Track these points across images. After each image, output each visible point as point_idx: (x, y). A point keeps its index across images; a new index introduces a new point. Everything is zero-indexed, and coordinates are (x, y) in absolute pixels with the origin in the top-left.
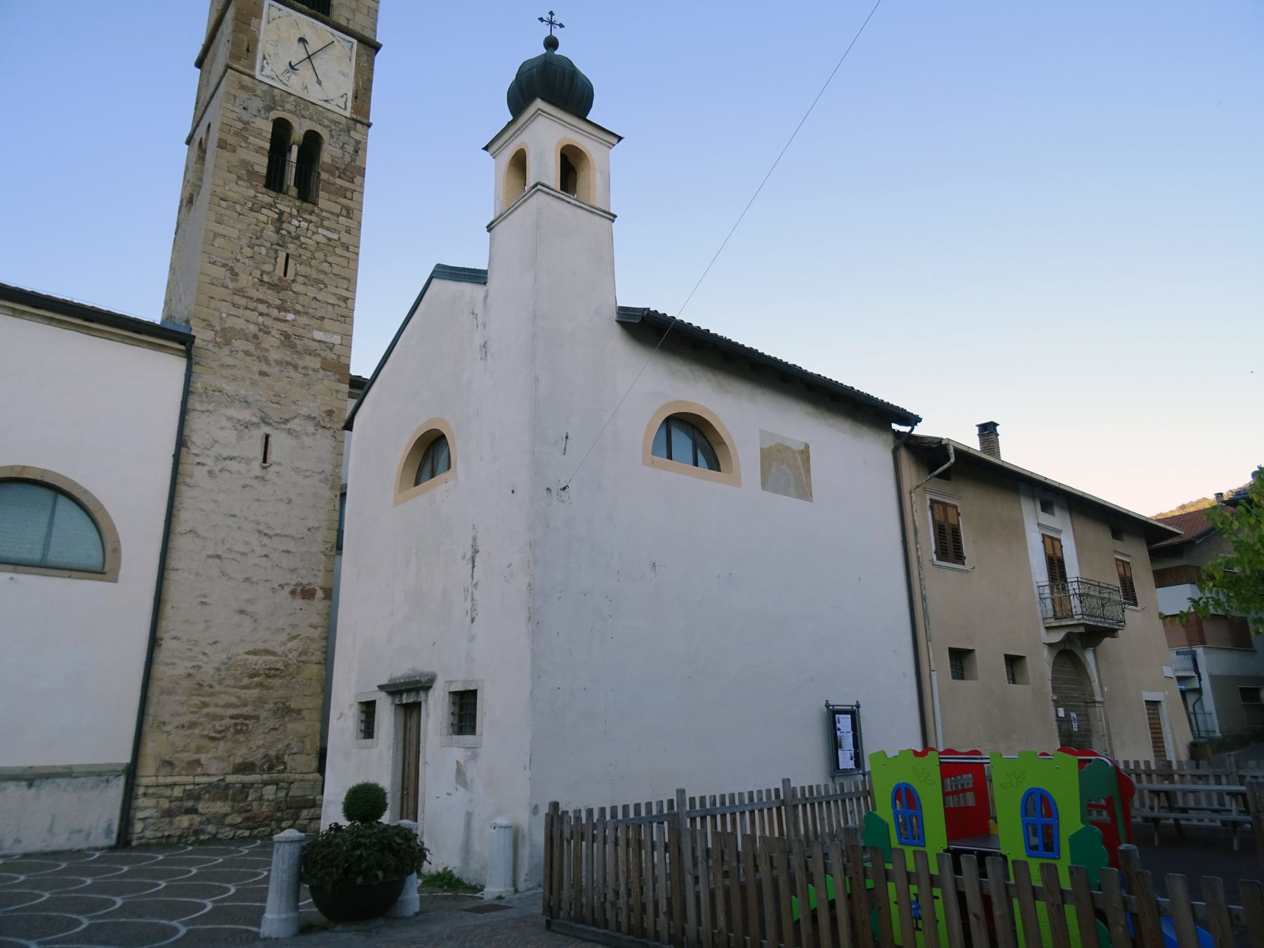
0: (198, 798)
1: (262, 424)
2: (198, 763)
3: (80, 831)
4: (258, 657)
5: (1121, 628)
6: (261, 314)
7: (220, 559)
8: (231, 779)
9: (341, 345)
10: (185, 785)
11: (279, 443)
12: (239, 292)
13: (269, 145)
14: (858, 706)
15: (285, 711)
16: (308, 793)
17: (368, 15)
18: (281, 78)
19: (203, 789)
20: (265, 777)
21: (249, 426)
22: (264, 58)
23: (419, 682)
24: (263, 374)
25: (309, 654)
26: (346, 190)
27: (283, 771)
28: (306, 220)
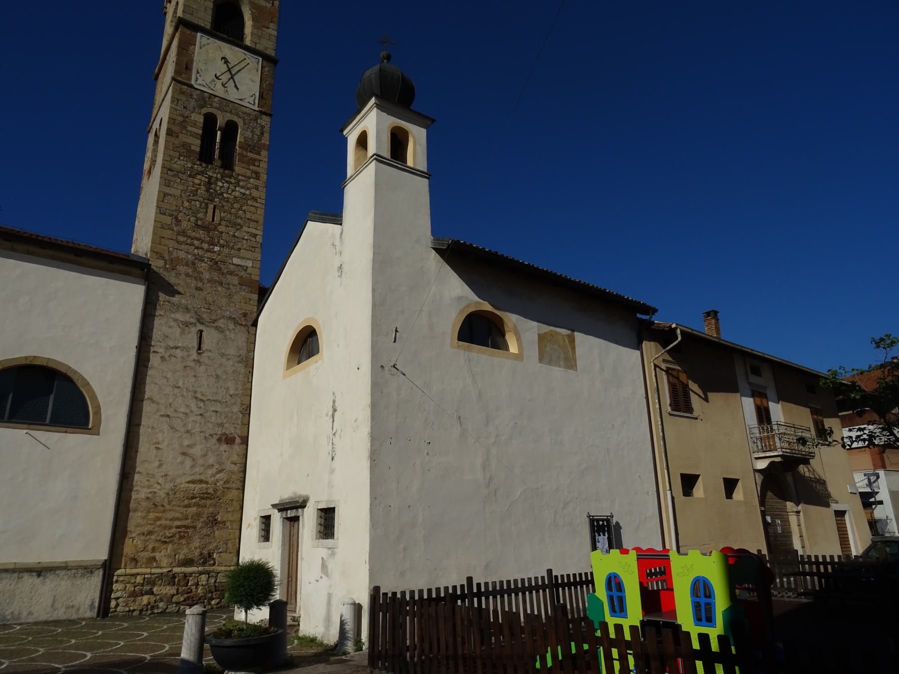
0: (154, 584)
1: (198, 324)
2: (154, 559)
3: (73, 607)
4: (195, 485)
5: (812, 458)
6: (197, 248)
8: (176, 570)
9: (252, 267)
10: (145, 574)
12: (183, 233)
13: (201, 131)
18: (210, 85)
19: (157, 577)
20: (200, 569)
21: (189, 325)
22: (198, 72)
23: (297, 502)
24: (198, 289)
26: (255, 160)
27: (214, 564)
28: (227, 182)
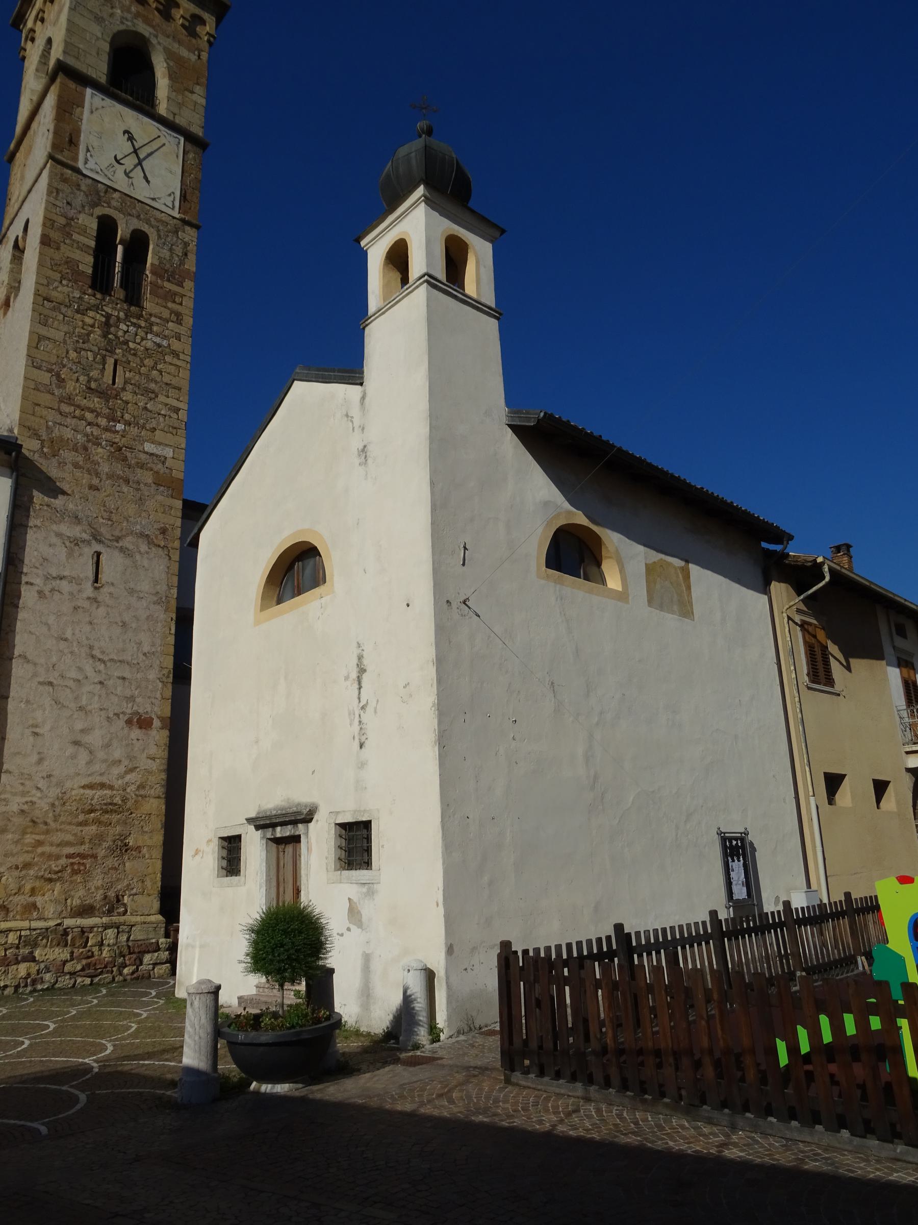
0: (35, 945)
1: (93, 541)
2: (34, 906)
4: (94, 792)
7: (52, 685)
8: (68, 922)
9: (173, 458)
11: (112, 564)
14: (747, 834)
15: (123, 848)
16: (151, 936)
17: (194, 111)
18: (106, 173)
19: (39, 934)
20: (105, 920)
22: (88, 150)
23: (299, 813)
25: (148, 787)
26: (175, 294)
28: (134, 325)
